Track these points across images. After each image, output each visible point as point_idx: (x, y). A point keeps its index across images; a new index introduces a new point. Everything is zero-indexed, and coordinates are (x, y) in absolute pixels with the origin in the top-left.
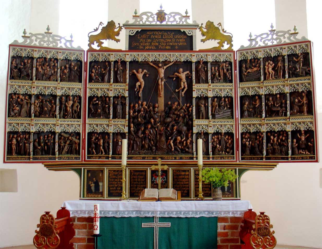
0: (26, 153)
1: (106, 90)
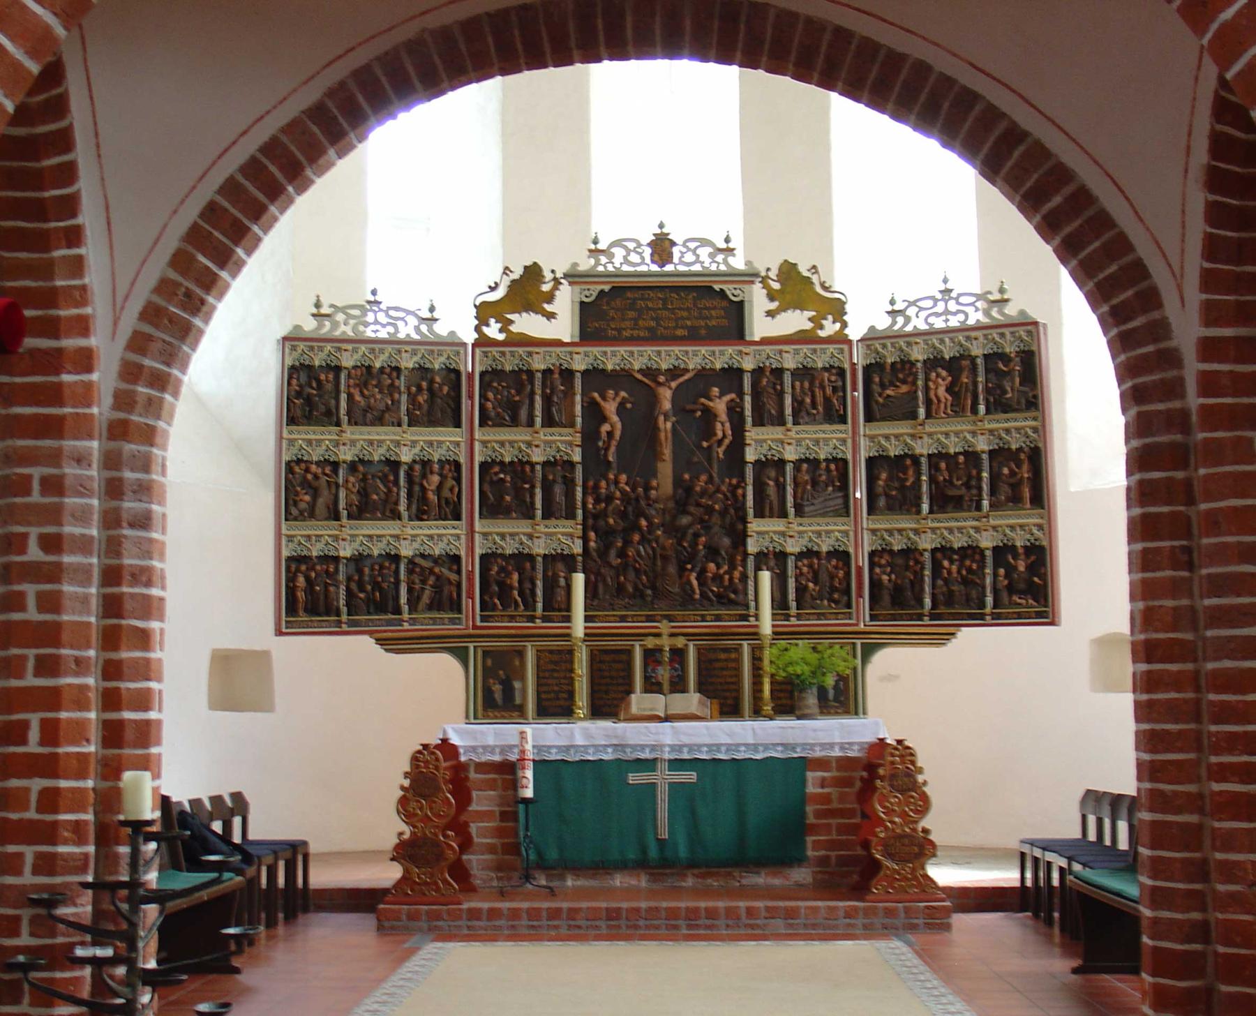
0: (333, 611)
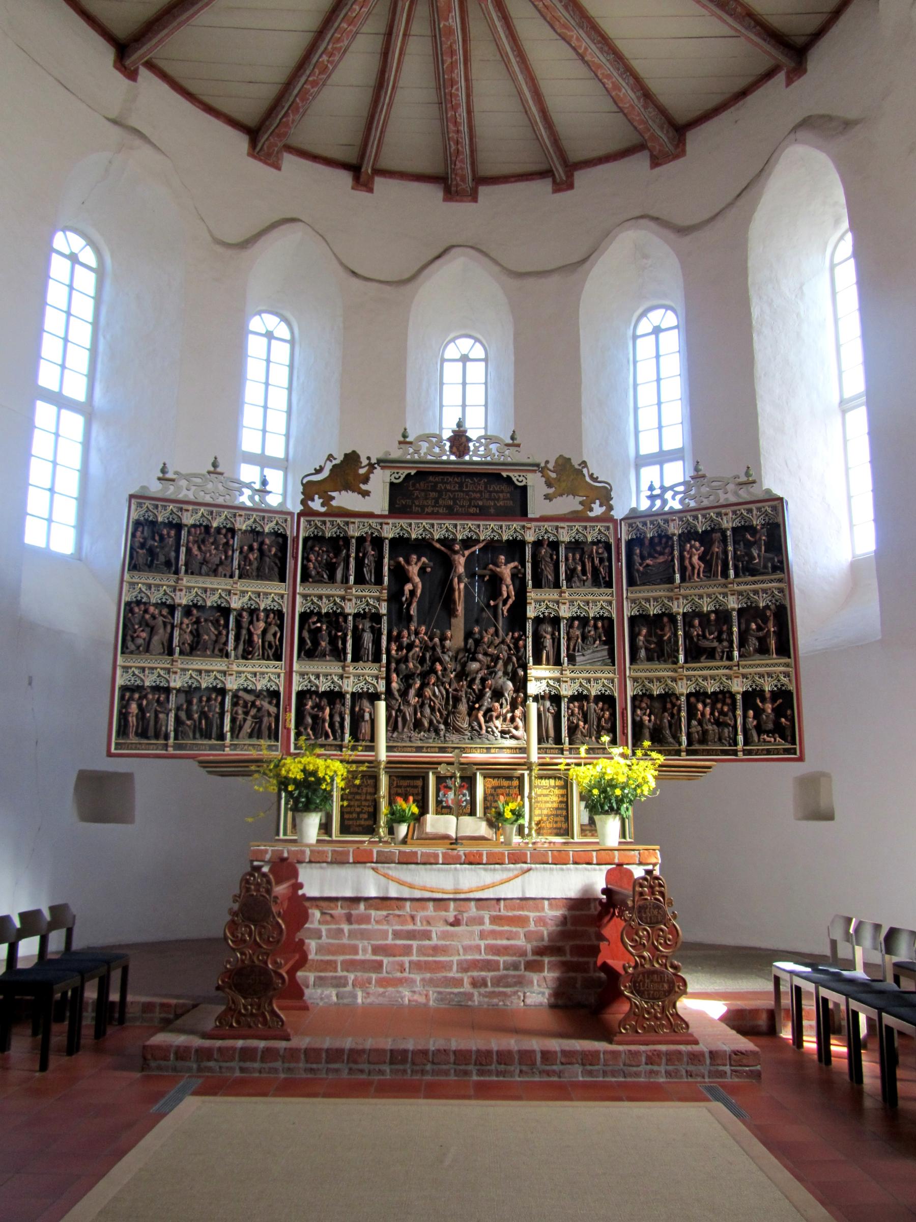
0: (159, 734)
1: (338, 600)
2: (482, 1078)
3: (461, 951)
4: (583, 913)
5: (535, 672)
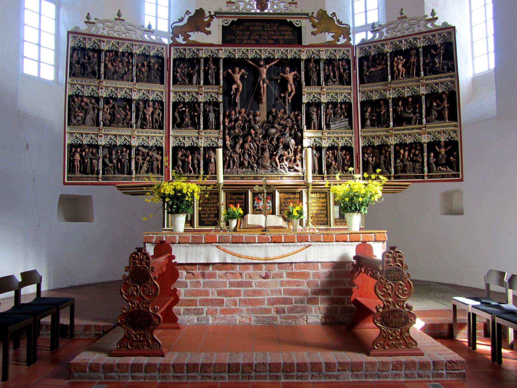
1: (194, 94)
2: (287, 381)
3: (270, 293)
4: (342, 270)
5: (307, 133)
